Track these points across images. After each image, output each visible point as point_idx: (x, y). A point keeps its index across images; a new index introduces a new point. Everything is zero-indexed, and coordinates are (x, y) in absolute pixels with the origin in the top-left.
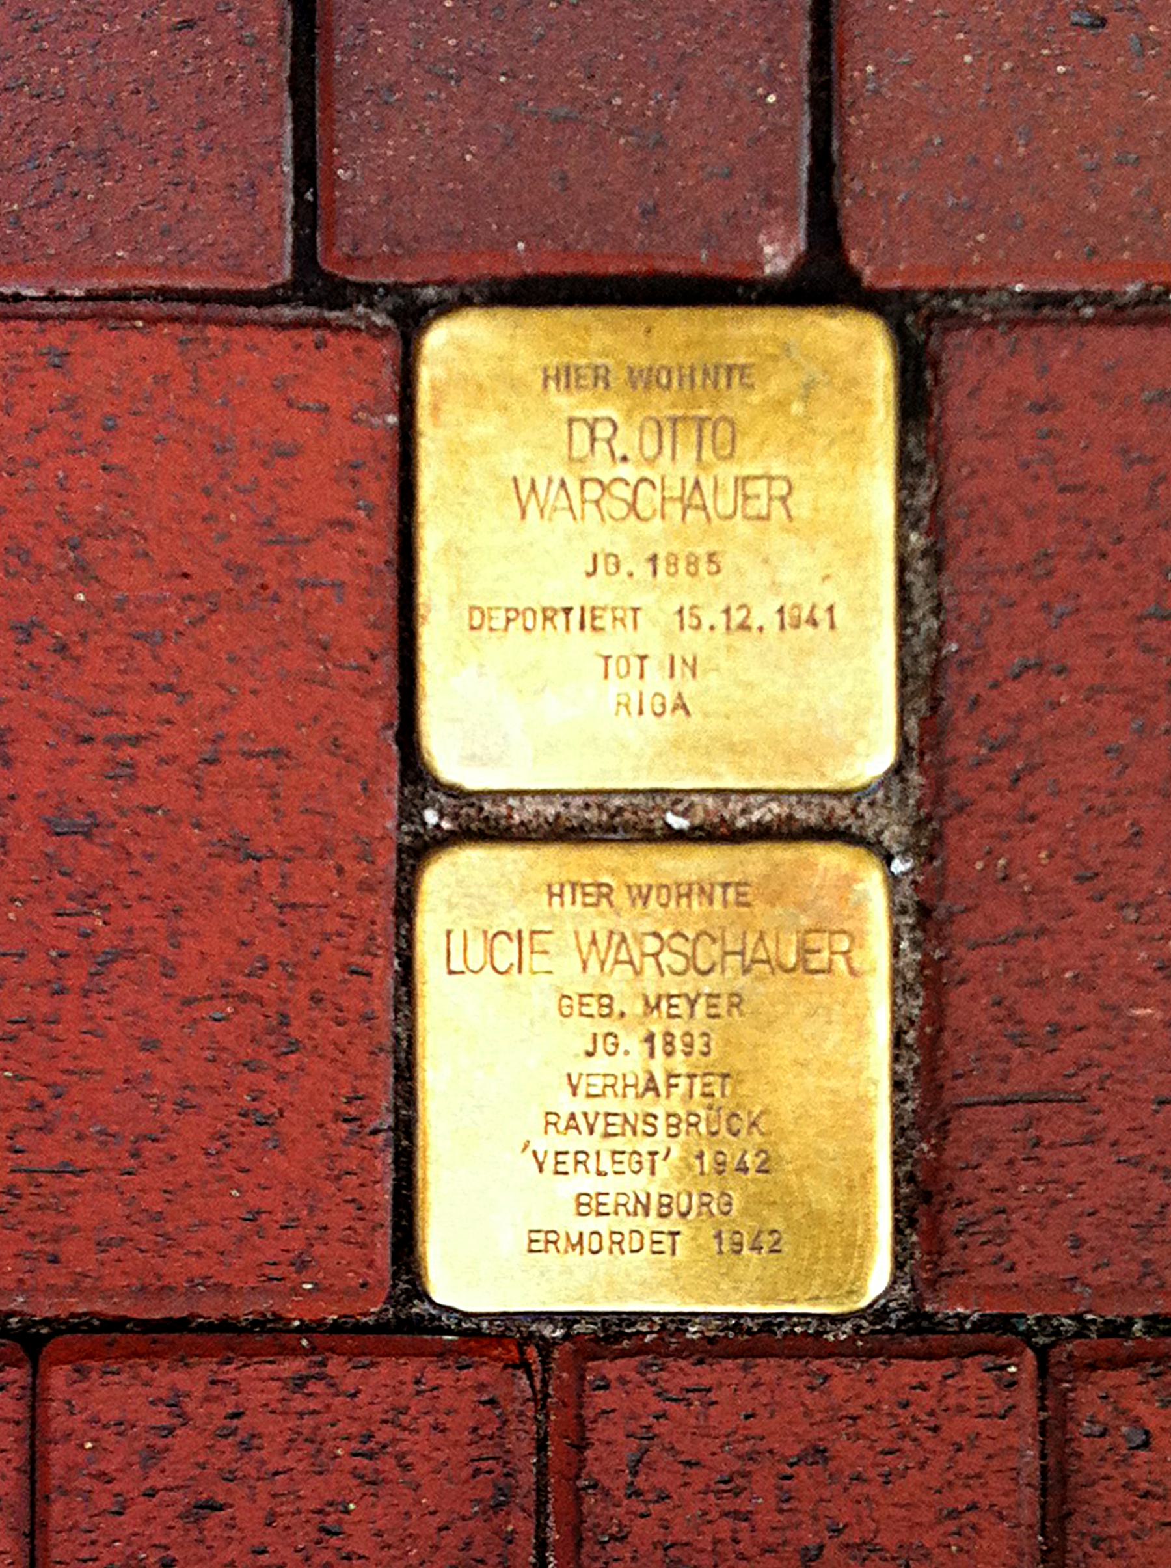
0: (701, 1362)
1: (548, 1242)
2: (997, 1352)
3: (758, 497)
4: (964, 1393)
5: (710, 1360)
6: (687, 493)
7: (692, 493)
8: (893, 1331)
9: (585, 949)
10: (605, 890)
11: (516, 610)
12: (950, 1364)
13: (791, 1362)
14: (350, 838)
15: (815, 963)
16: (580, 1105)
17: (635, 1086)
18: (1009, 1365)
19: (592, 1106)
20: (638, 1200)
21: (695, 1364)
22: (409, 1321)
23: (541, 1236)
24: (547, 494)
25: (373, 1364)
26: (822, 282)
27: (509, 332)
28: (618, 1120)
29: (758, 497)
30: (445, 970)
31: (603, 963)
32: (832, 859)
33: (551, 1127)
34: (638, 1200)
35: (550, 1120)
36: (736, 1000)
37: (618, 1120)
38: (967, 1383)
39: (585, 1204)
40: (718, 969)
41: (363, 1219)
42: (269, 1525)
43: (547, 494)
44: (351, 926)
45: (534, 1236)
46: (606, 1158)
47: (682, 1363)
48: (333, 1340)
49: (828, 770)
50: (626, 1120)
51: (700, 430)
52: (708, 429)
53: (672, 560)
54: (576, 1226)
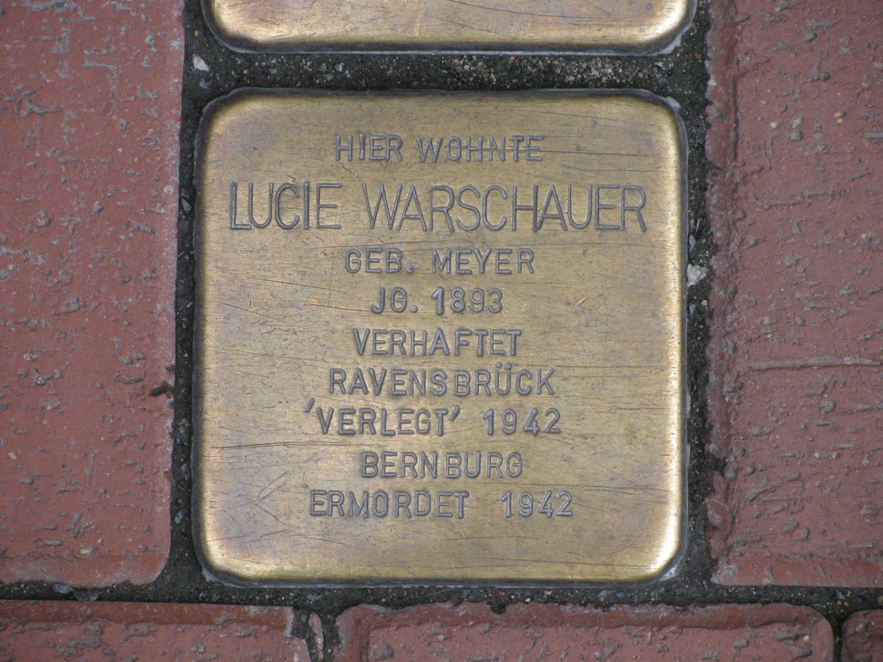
1: (394, 343)
2: (792, 622)
9: (373, 204)
10: (395, 144)
12: (748, 632)
15: (610, 218)
16: (366, 364)
17: (424, 344)
18: (804, 635)
19: (379, 365)
20: (425, 461)
22: (189, 582)
23: (387, 338)
25: (150, 633)
28: (406, 379)
31: (392, 220)
33: (337, 387)
34: (425, 461)
35: (335, 380)
37: (406, 379)
39: (370, 465)
40: (509, 226)
42: (423, 162)
45: (319, 498)
46: (392, 417)
48: (109, 608)
50: (413, 379)
53: (511, 419)
54: (359, 487)
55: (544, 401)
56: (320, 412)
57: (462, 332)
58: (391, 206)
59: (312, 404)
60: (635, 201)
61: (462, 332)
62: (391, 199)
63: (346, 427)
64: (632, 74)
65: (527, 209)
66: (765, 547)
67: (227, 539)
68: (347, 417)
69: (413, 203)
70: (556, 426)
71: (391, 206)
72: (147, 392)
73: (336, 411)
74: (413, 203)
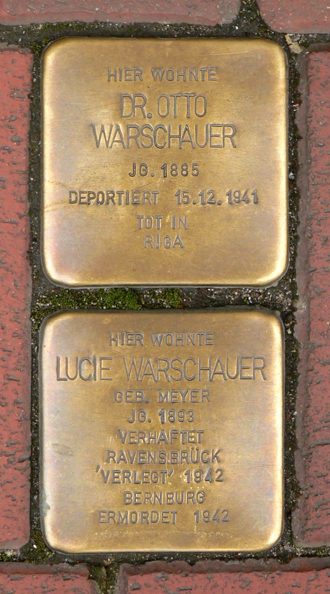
0: (187, 576)
3: (218, 136)
4: (318, 588)
5: (192, 575)
6: (182, 133)
7: (184, 133)
8: (280, 557)
11: (93, 193)
13: (232, 575)
14: (8, 310)
15: (247, 374)
21: (183, 577)
22: (37, 553)
24: (110, 133)
26: (251, 26)
27: (22, 213)
29: (218, 136)
30: (56, 378)
32: (256, 318)
36: (206, 393)
38: (320, 583)
41: (15, 506)
43: (110, 133)
44: (9, 355)
47: (177, 576)
49: (48, 213)
51: (188, 101)
52: (192, 100)
55: (216, 465)
56: (102, 472)
57: (175, 432)
58: (107, 135)
59: (98, 467)
60: (260, 364)
61: (175, 432)
62: (107, 132)
63: (116, 479)
64: (261, 301)
65: (173, 137)
66: (322, 532)
67: (57, 535)
68: (116, 474)
69: (118, 134)
70: (221, 478)
71: (107, 135)
72: (17, 461)
73: (111, 472)
74: (118, 134)
